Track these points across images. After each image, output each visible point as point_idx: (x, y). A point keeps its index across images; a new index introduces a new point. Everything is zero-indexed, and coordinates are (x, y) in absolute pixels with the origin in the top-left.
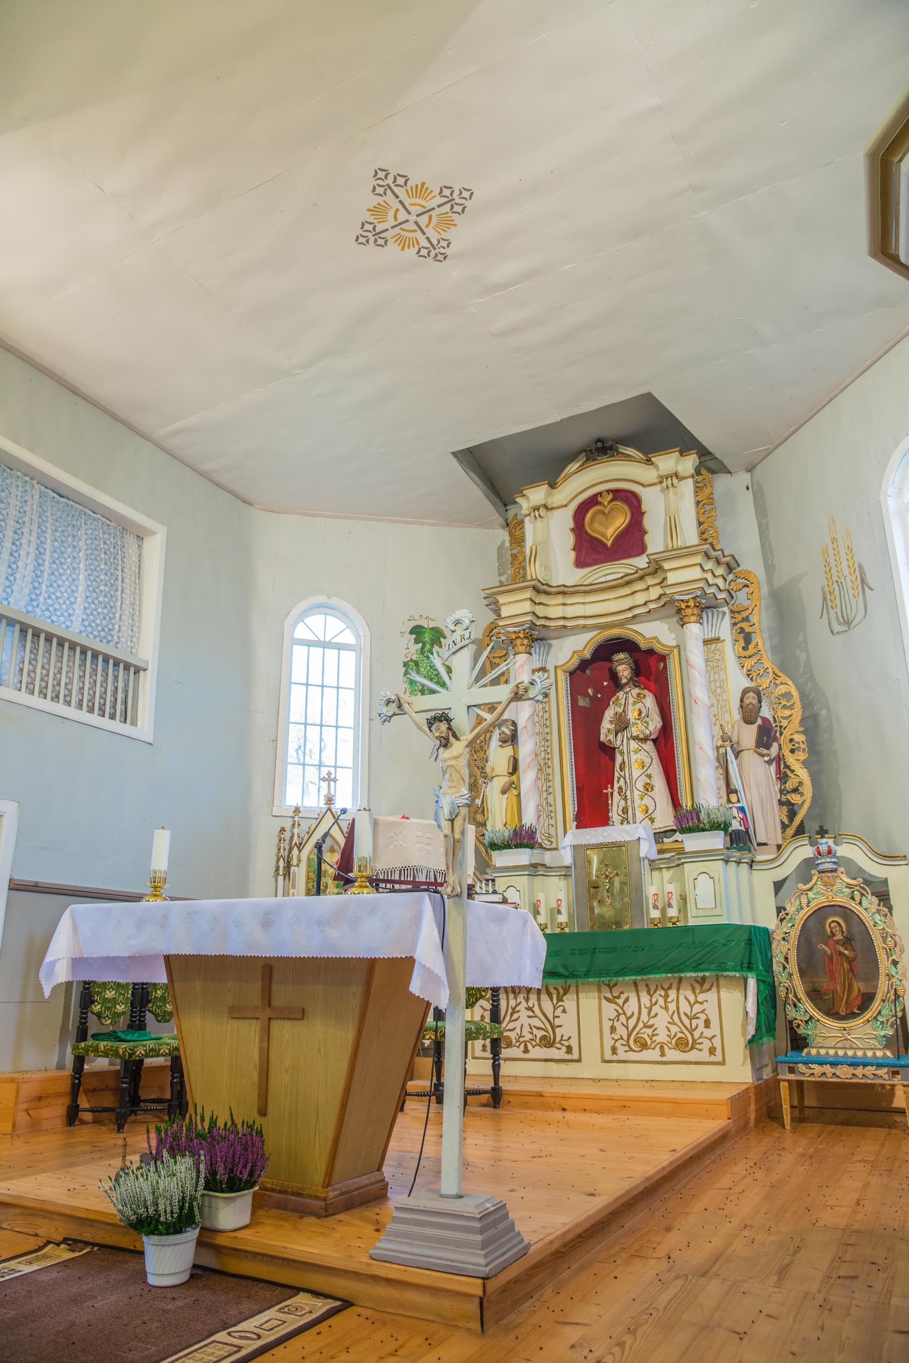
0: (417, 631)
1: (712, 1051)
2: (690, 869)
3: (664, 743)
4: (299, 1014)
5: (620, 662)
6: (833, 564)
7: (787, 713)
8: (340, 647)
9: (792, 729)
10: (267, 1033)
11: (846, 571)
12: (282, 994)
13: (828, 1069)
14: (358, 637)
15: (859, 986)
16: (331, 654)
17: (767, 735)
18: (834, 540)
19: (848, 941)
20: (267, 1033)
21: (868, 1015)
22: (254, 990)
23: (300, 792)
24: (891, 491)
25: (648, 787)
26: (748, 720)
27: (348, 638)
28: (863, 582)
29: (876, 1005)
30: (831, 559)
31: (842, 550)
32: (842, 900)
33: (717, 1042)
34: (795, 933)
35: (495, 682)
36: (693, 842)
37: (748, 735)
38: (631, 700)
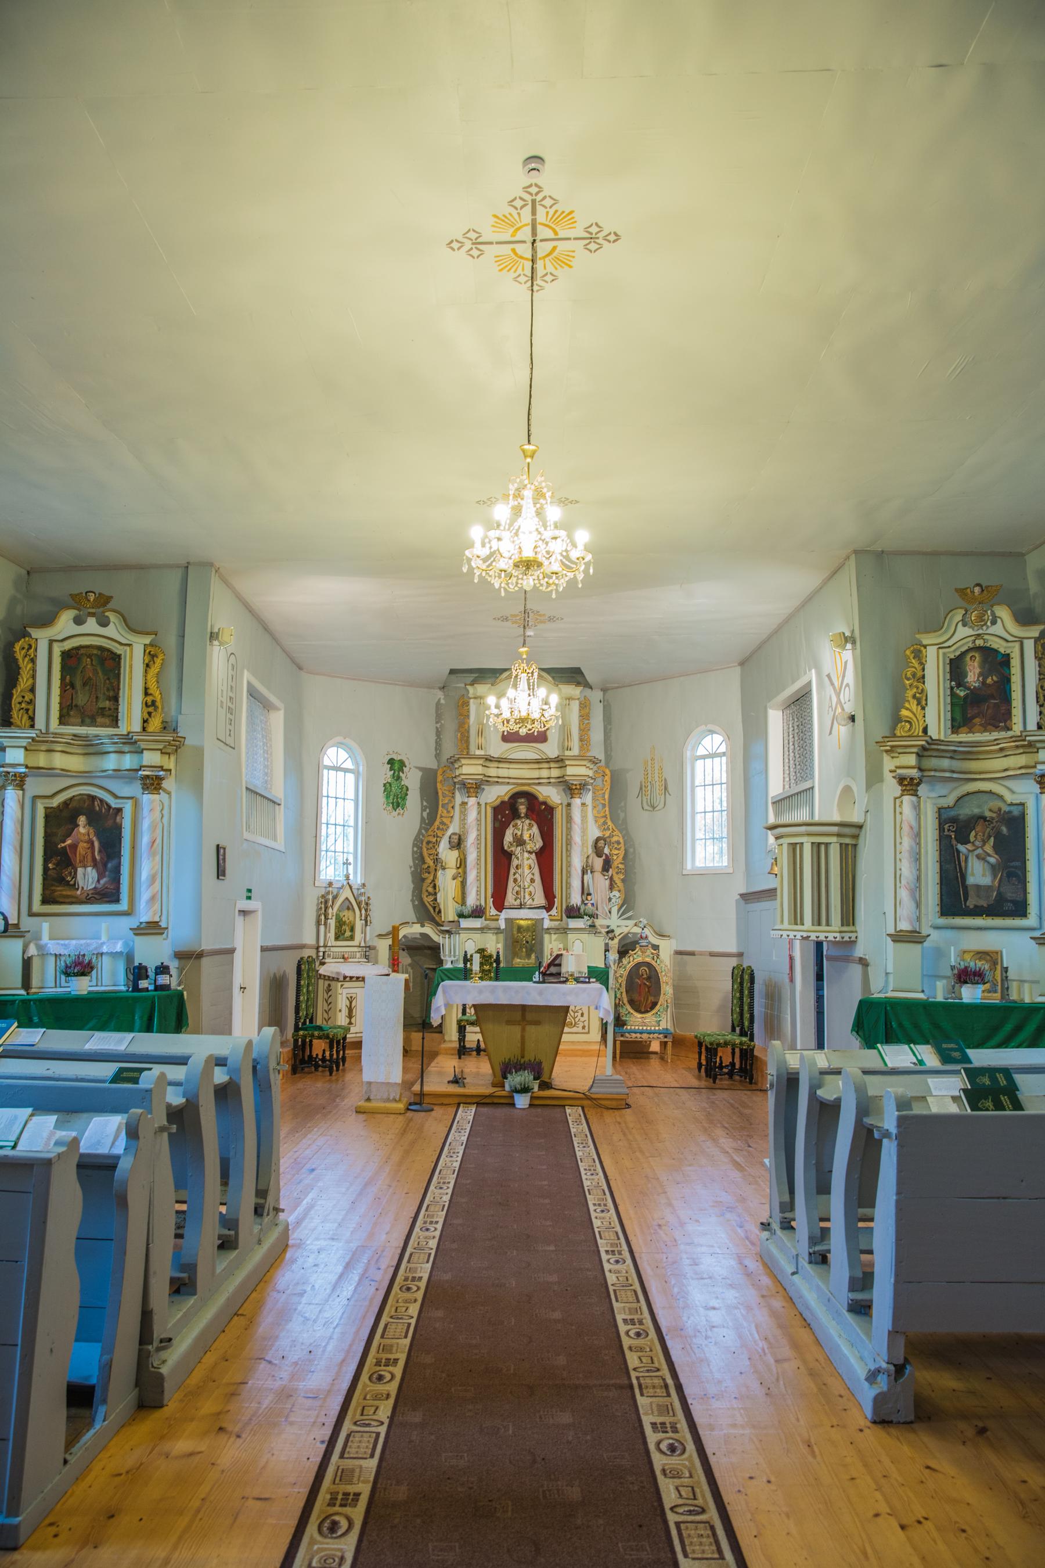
0: (391, 762)
1: (584, 1027)
2: (571, 937)
3: (545, 857)
4: (537, 1023)
5: (522, 804)
6: (649, 772)
7: (616, 852)
8: (346, 770)
9: (617, 862)
10: (523, 1030)
11: (657, 779)
12: (529, 1016)
13: (638, 1035)
14: (357, 764)
15: (651, 999)
16: (341, 774)
17: (607, 866)
18: (652, 759)
19: (649, 978)
20: (523, 1030)
21: (654, 1011)
22: (518, 1015)
23: (329, 871)
24: (690, 748)
25: (532, 881)
26: (599, 855)
27: (349, 765)
28: (666, 788)
29: (658, 1007)
30: (649, 768)
31: (656, 768)
32: (648, 960)
33: (586, 1024)
34: (626, 974)
35: (628, 918)
36: (573, 923)
37: (598, 863)
38: (526, 827)
